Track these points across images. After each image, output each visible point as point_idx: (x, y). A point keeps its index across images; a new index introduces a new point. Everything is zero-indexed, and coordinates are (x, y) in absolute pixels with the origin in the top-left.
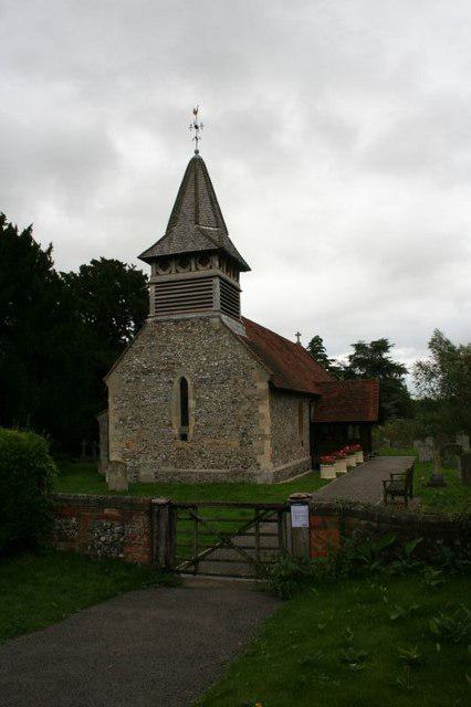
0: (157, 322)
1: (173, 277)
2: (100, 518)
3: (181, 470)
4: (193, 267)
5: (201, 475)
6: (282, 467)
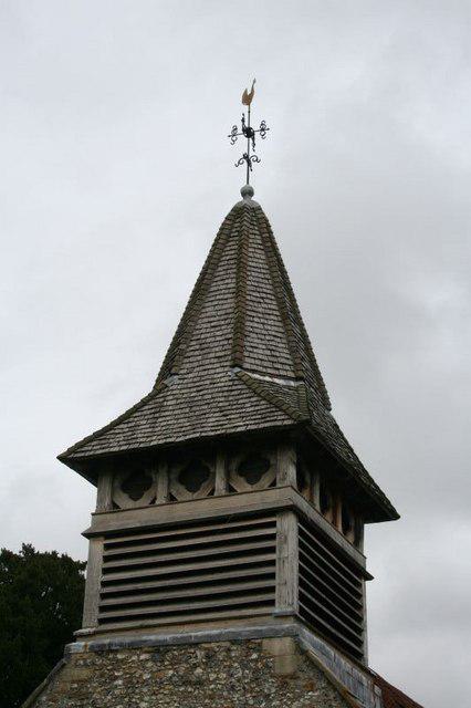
0: (101, 651)
4: (220, 484)
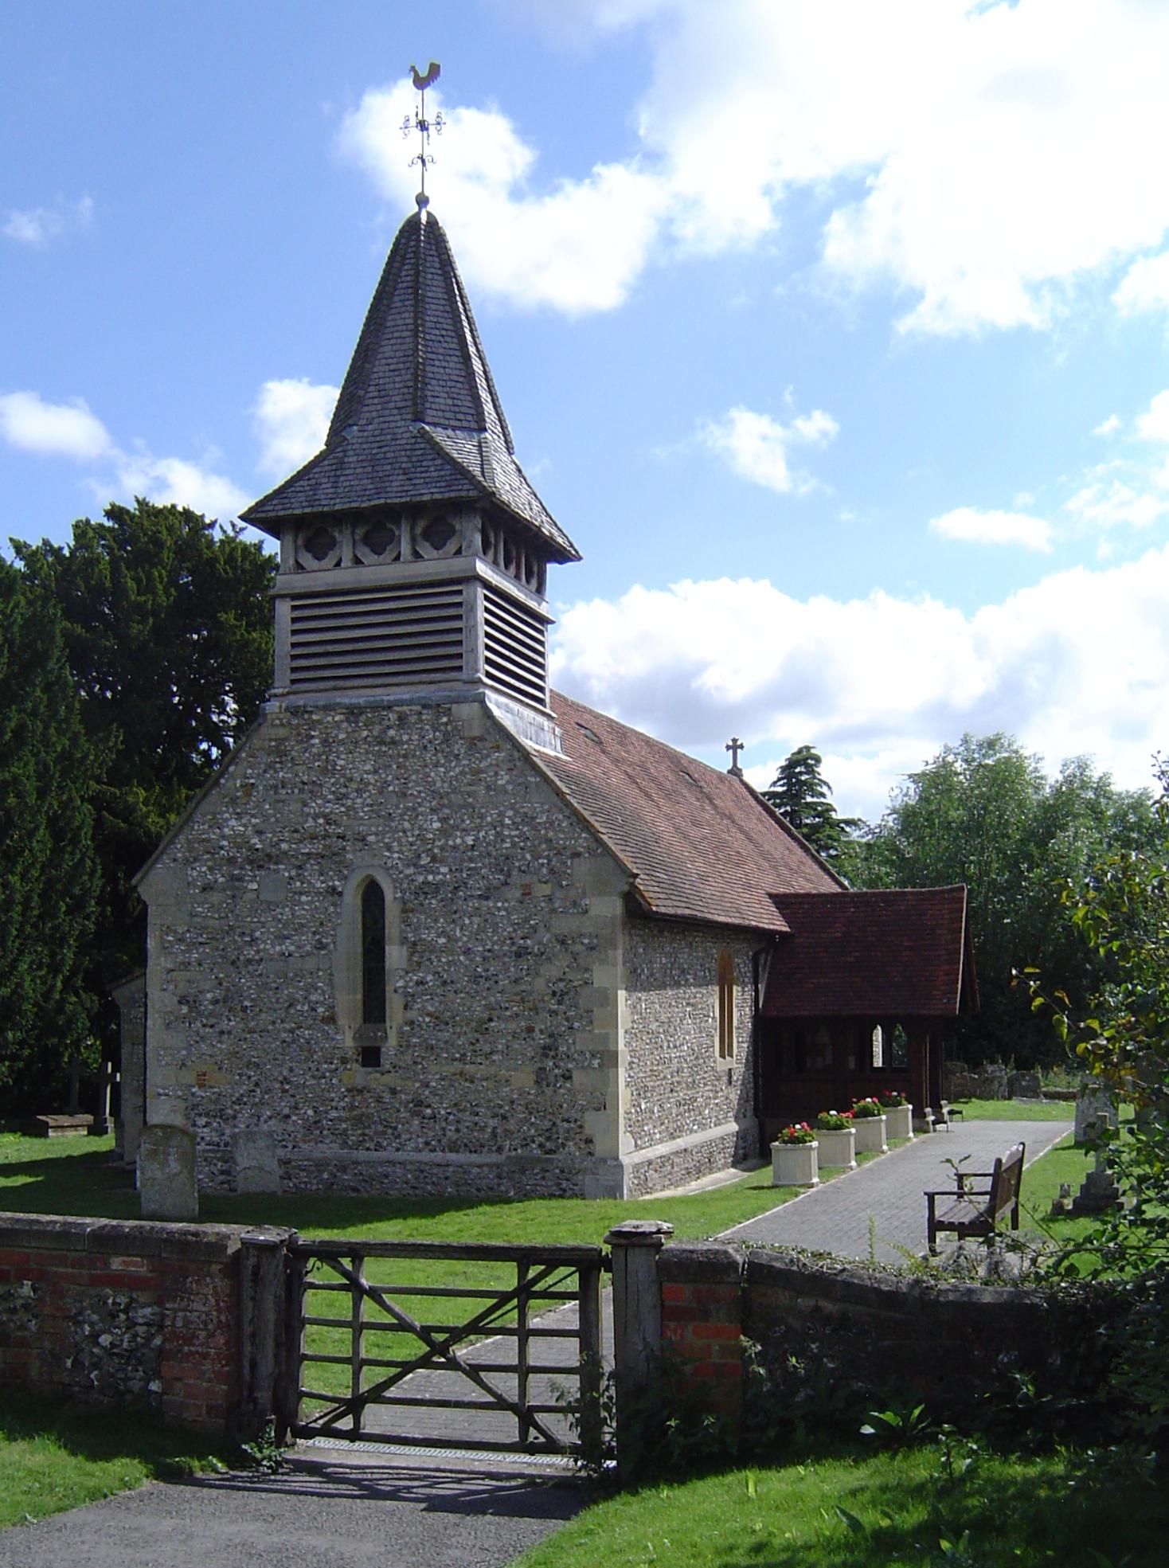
0: (295, 711)
1: (347, 576)
2: (96, 1281)
3: (361, 1155)
4: (405, 548)
5: (421, 1169)
6: (663, 1149)
